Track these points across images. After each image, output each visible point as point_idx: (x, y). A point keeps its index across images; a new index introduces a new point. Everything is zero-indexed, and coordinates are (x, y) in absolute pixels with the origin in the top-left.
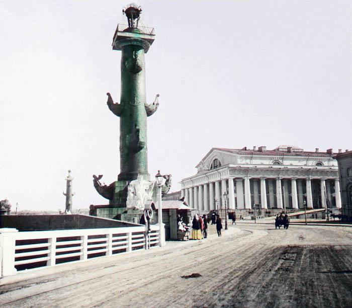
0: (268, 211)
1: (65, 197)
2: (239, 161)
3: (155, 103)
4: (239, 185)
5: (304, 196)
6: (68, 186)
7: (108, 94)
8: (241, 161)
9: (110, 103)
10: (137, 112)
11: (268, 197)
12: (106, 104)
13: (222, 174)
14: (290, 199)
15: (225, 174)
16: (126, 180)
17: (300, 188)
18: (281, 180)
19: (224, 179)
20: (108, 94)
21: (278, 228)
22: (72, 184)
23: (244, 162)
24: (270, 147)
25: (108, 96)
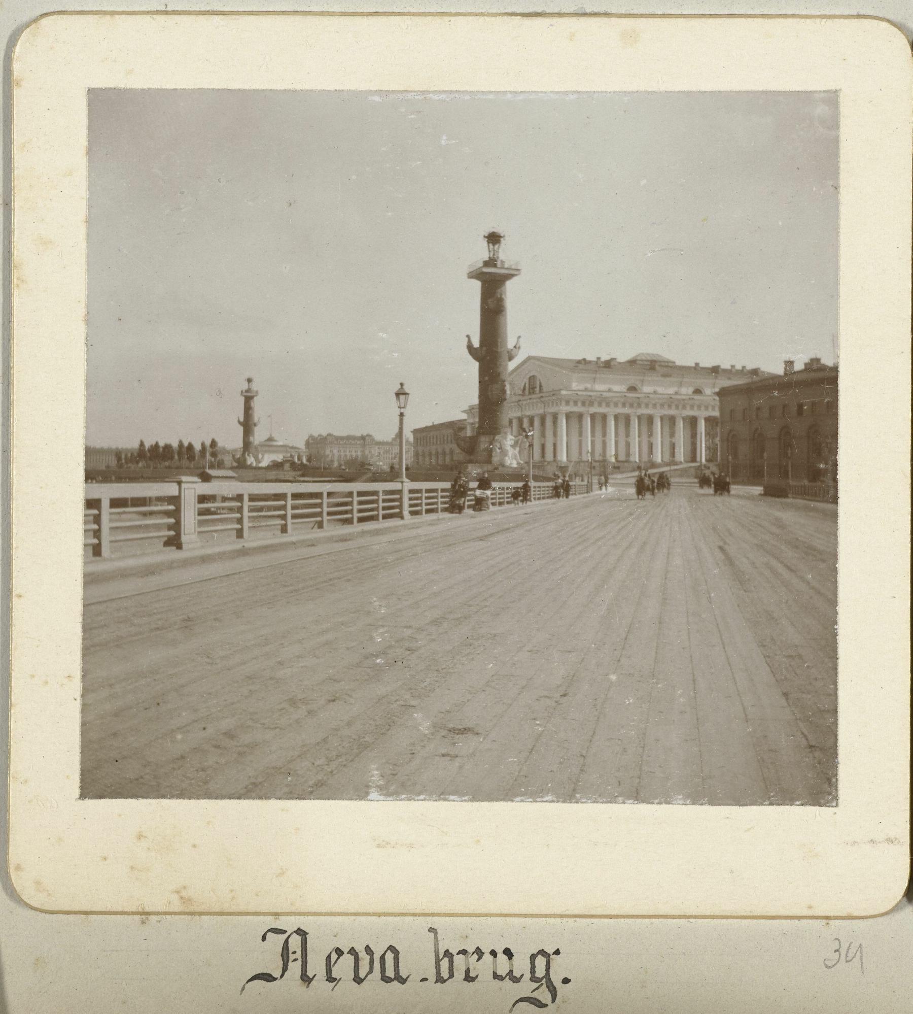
0: (616, 465)
1: (241, 429)
2: (575, 386)
3: (517, 346)
4: (574, 423)
5: (649, 442)
6: (248, 409)
7: (468, 336)
8: (577, 386)
9: (470, 347)
10: (499, 340)
11: (616, 442)
12: (466, 347)
13: (524, 407)
14: (673, 447)
15: (515, 411)
16: (802, 409)
17: (667, 429)
18: (590, 415)
19: (529, 416)
20: (468, 336)
21: (640, 497)
22: (256, 404)
23: (581, 387)
24: (623, 356)
25: (467, 339)
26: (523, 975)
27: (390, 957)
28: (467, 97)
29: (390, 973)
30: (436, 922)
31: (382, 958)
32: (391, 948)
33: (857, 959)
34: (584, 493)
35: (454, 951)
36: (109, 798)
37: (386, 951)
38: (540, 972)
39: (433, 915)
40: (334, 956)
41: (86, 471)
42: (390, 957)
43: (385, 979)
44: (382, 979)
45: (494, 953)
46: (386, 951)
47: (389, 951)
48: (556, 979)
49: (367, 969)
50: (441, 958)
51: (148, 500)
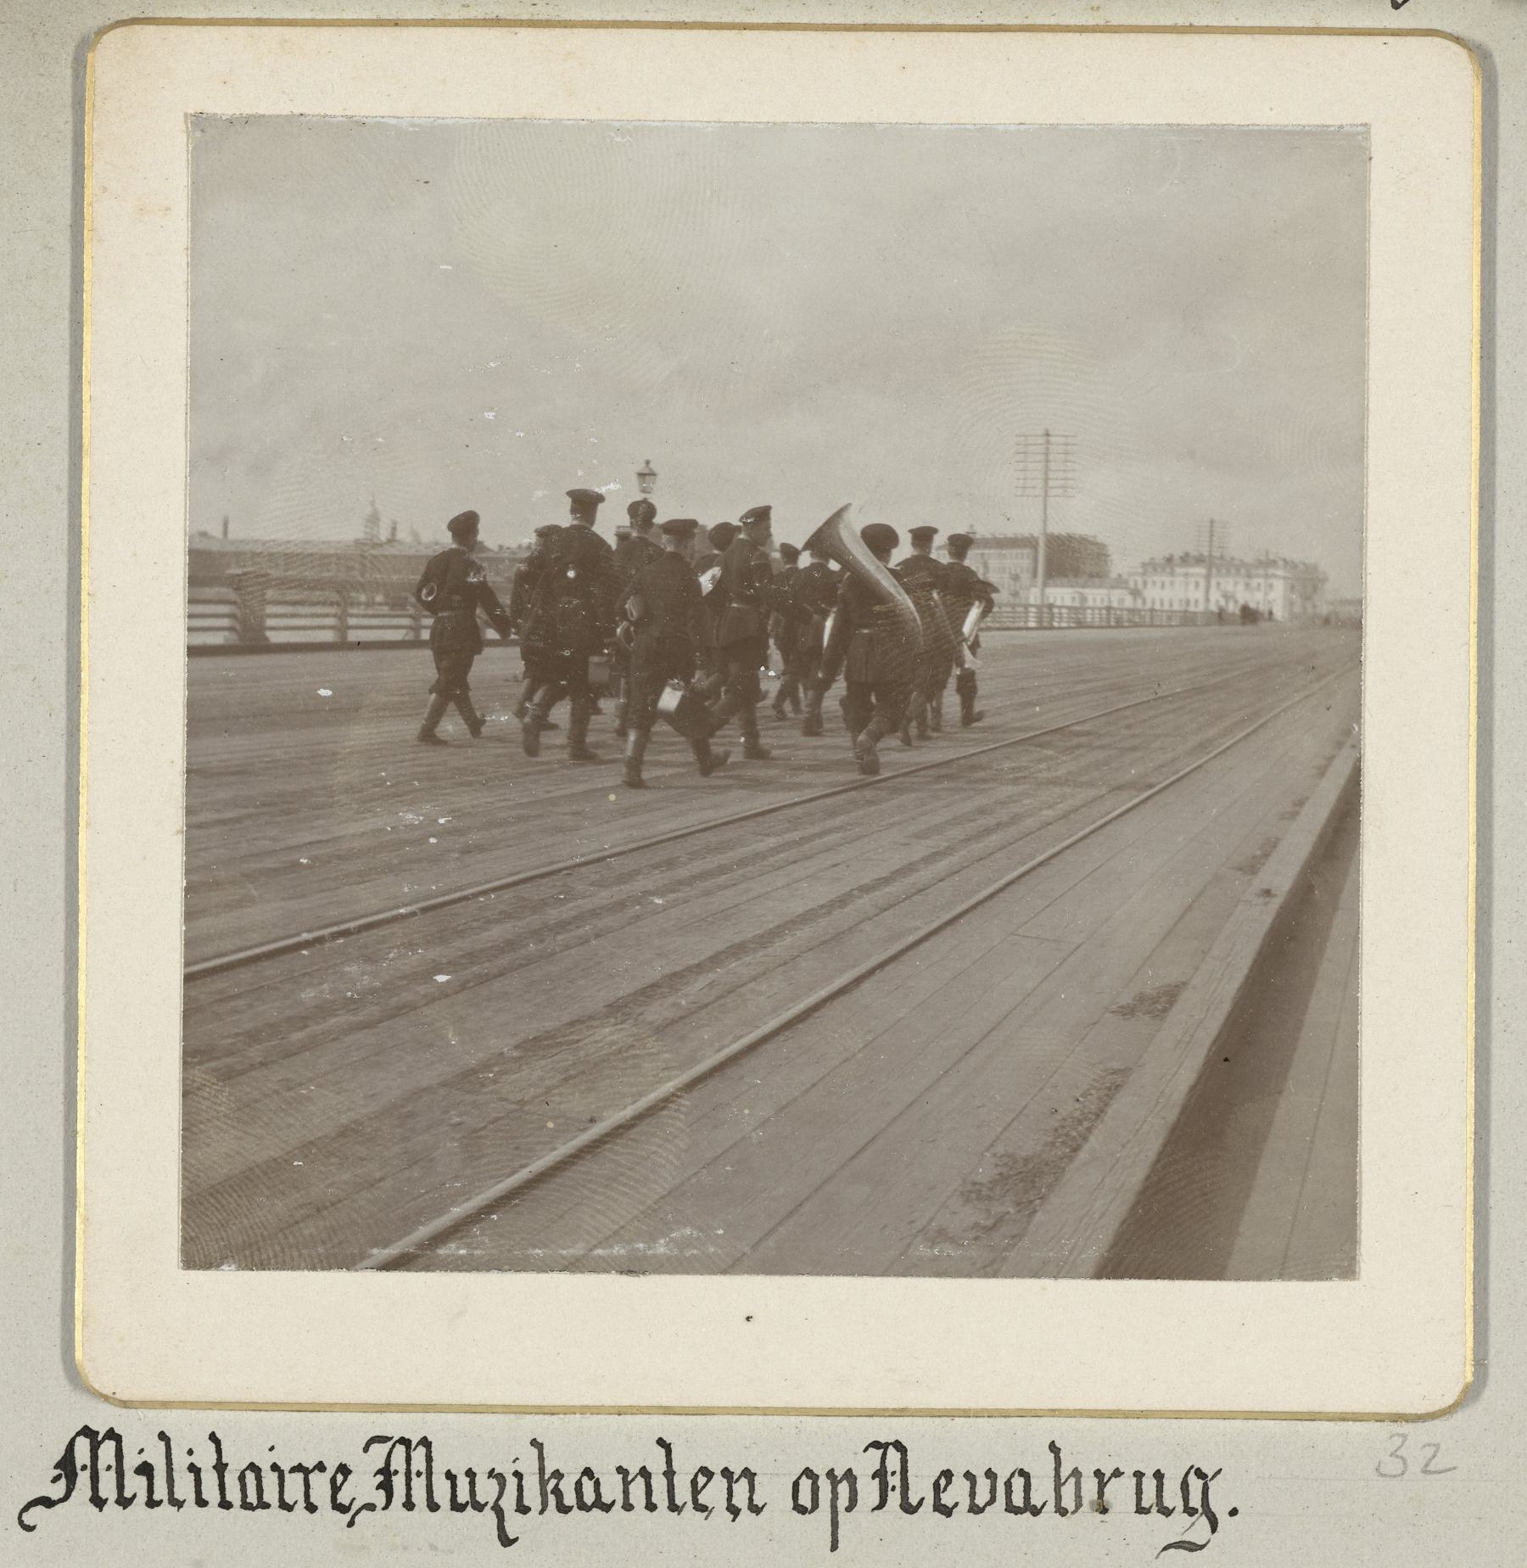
26: (956, 1504)
27: (1018, 1483)
28: (762, 126)
29: (1018, 1500)
30: (668, 1428)
31: (1008, 1484)
32: (1023, 1473)
33: (1065, 1472)
34: (282, 583)
35: (286, 1467)
36: (452, 1271)
37: (799, 1478)
38: (1195, 1501)
39: (166, 1405)
40: (340, 1478)
41: (192, 706)
42: (1018, 1483)
43: (1011, 1508)
44: (795, 1508)
45: (969, 1476)
46: (799, 1478)
47: (804, 1477)
48: (1219, 1506)
49: (987, 1497)
50: (1063, 1481)
51: (228, 748)
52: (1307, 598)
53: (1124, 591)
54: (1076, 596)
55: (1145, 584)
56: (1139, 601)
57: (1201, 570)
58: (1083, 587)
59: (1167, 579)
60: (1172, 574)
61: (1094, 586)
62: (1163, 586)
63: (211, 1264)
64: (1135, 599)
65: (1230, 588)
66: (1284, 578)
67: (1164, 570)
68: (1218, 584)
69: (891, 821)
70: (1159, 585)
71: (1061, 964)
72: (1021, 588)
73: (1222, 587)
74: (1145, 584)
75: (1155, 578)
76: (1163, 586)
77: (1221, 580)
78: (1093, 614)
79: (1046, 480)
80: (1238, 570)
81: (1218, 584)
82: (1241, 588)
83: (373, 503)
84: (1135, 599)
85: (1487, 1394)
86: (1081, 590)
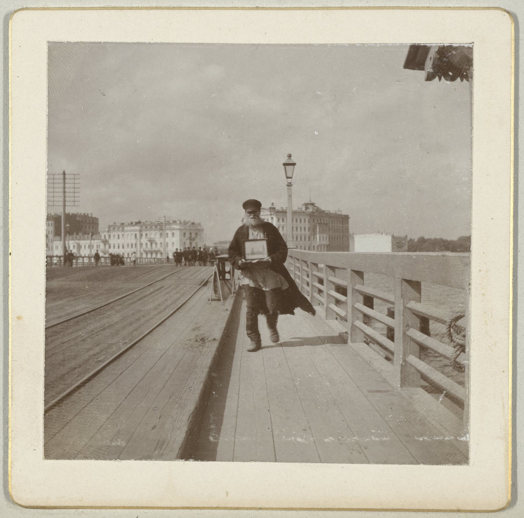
52: (191, 239)
53: (100, 241)
54: (76, 245)
55: (110, 236)
56: (107, 246)
57: (137, 228)
58: (79, 240)
59: (121, 234)
60: (123, 230)
61: (84, 239)
62: (119, 238)
63: (46, 451)
64: (105, 245)
65: (152, 236)
66: (180, 229)
67: (118, 229)
68: (146, 235)
69: (409, 349)
70: (116, 236)
71: (81, 411)
72: (222, 261)
73: (149, 236)
74: (110, 236)
75: (115, 233)
76: (119, 238)
77: (148, 232)
78: (145, 260)
79: (64, 183)
80: (156, 227)
81: (146, 235)
82: (158, 236)
83: (97, 251)
84: (105, 245)
85: (518, 502)
86: (78, 242)
